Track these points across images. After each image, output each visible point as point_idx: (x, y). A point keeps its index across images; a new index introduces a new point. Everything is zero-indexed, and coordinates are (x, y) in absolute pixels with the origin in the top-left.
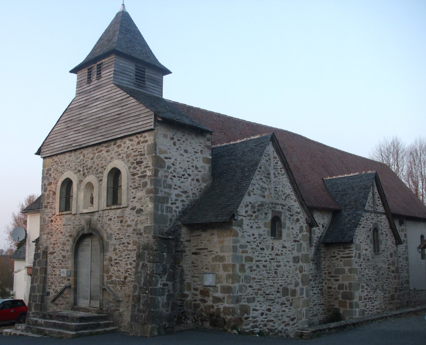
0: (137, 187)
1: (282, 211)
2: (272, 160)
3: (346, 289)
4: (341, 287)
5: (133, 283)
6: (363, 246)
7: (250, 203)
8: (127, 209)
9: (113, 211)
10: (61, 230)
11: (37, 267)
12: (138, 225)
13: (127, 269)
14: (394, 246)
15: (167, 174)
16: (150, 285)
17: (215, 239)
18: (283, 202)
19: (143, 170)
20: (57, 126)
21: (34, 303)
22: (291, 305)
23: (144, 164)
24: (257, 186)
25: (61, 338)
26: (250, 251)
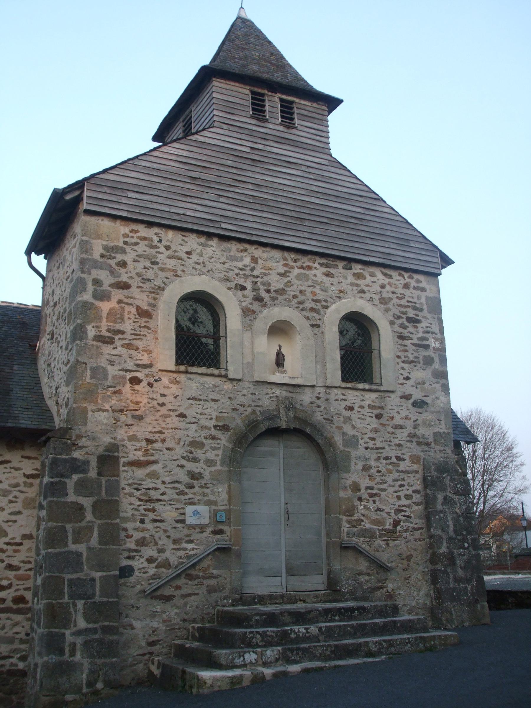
0: (412, 362)
8: (393, 396)
9: (356, 393)
13: (399, 506)
19: (421, 335)
21: (80, 604)
25: (430, 649)
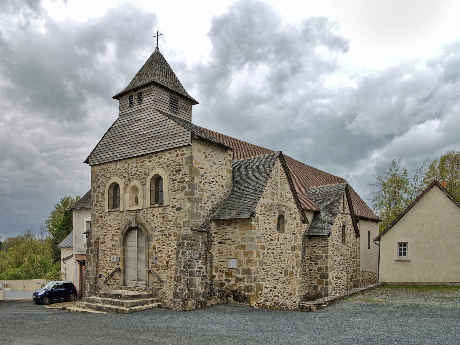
0: (177, 190)
1: (285, 211)
2: (279, 171)
3: (323, 271)
4: (319, 269)
5: (174, 267)
6: (336, 238)
7: (264, 204)
8: (168, 207)
9: (156, 209)
10: (111, 224)
11: (90, 254)
12: (178, 220)
14: (355, 238)
15: (201, 181)
16: (189, 268)
17: (238, 231)
18: (286, 204)
20: (103, 141)
22: (289, 283)
23: (182, 172)
24: (269, 191)
26: (263, 241)
